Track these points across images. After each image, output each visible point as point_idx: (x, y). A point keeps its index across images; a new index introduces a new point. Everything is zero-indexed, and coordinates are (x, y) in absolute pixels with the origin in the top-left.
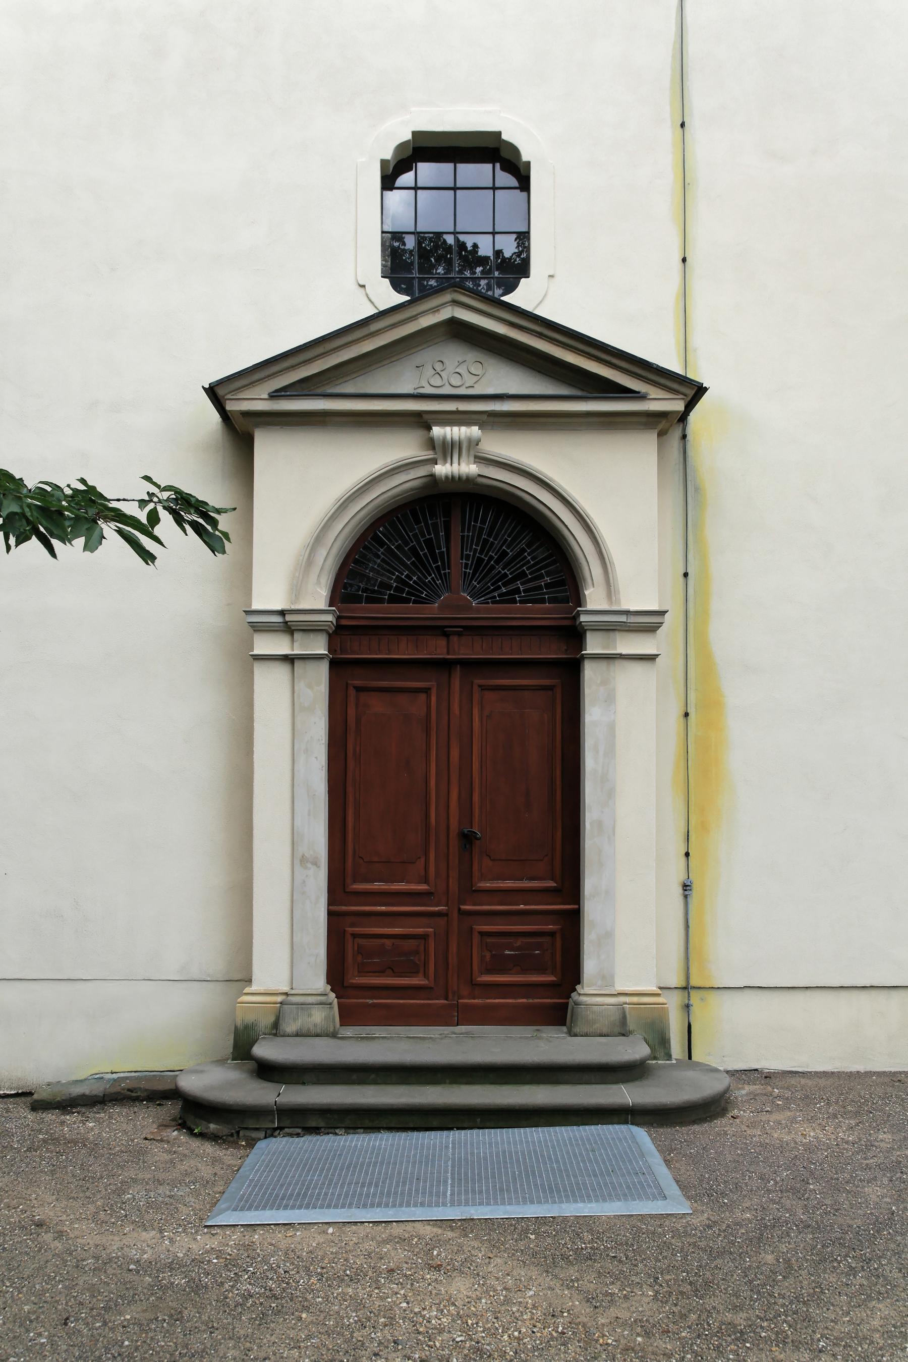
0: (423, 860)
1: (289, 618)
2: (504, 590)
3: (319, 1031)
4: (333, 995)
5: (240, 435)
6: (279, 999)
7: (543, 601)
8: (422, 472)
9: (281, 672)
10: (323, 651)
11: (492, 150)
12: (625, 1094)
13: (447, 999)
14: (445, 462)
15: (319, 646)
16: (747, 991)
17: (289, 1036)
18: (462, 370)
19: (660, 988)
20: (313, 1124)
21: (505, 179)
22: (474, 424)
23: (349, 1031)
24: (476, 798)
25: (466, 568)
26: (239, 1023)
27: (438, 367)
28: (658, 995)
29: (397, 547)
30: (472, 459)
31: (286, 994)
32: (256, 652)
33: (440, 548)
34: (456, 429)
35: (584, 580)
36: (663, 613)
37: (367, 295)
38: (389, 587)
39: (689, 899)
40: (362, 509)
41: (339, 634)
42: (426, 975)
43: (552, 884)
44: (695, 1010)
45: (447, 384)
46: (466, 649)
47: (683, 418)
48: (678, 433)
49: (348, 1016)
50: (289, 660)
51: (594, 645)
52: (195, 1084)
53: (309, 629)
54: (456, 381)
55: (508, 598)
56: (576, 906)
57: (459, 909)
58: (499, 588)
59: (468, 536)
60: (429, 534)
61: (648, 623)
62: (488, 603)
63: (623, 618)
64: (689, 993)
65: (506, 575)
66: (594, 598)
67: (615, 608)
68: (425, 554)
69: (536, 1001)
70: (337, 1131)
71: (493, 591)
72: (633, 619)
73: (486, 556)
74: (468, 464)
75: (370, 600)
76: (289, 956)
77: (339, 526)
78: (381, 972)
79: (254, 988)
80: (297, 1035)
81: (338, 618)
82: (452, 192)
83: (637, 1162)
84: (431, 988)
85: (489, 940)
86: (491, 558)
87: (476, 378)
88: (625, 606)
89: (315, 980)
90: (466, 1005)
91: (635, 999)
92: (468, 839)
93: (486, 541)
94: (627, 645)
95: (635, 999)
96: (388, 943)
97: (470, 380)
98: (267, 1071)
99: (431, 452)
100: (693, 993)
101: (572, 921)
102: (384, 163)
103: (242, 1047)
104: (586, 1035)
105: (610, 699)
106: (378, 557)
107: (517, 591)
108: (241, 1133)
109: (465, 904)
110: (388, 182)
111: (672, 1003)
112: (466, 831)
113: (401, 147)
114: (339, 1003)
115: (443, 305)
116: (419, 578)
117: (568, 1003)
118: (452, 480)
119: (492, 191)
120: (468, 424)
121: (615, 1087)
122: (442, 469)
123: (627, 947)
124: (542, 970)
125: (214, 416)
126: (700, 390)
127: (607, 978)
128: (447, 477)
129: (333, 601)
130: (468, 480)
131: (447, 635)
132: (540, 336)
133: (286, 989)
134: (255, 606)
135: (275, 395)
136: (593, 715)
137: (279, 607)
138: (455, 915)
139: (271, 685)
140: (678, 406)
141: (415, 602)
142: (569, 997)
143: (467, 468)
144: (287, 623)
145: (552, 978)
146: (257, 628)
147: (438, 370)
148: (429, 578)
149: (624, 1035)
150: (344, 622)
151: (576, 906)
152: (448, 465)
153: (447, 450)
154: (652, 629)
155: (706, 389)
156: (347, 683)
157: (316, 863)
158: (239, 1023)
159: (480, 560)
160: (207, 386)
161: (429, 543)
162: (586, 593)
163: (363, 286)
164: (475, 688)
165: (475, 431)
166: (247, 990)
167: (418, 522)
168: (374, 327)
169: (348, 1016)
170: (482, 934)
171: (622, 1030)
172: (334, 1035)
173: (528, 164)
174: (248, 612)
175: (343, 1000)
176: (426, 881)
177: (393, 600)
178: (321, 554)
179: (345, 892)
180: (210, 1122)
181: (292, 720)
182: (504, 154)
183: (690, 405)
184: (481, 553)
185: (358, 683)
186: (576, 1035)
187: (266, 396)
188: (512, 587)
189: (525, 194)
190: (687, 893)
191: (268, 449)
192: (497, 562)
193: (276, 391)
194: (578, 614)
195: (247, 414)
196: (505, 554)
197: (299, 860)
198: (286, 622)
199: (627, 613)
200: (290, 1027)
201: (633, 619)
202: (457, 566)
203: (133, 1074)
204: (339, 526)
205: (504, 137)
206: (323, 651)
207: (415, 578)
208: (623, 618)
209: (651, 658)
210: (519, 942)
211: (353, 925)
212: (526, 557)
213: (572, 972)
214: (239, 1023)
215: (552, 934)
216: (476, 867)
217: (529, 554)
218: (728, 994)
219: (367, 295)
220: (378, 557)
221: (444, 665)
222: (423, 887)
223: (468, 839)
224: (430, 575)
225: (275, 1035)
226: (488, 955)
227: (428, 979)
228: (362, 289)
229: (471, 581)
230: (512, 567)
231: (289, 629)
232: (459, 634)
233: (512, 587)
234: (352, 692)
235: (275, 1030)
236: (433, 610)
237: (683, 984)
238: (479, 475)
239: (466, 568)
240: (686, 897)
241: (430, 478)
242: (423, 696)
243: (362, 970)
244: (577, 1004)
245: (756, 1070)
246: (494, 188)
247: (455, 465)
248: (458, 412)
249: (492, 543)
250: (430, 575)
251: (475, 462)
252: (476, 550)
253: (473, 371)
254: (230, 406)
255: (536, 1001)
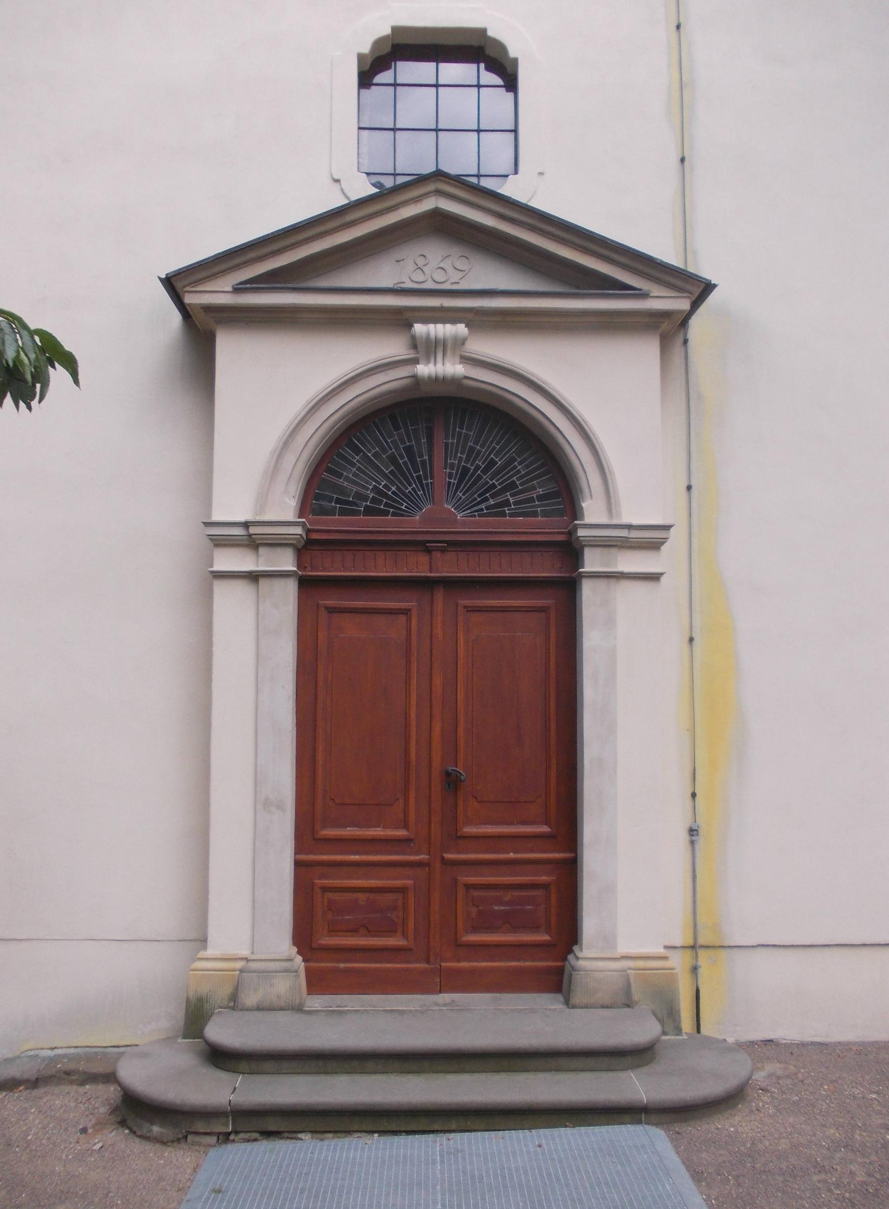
0: (401, 801)
1: (253, 530)
2: (492, 502)
3: (283, 1004)
4: (299, 959)
5: (200, 334)
6: (239, 965)
7: (535, 514)
8: (403, 372)
9: (241, 591)
10: (291, 567)
11: (475, 49)
12: (635, 1086)
13: (428, 962)
14: (428, 362)
15: (286, 561)
16: (759, 950)
17: (248, 1010)
18: (446, 264)
19: (666, 947)
20: (272, 1128)
21: (489, 78)
22: (460, 322)
23: (316, 1002)
24: (461, 731)
25: (450, 478)
26: (191, 994)
27: (421, 262)
28: (665, 958)
29: (376, 455)
30: (457, 359)
31: (247, 959)
32: (216, 568)
33: (421, 456)
34: (440, 326)
35: (581, 492)
36: (667, 528)
37: (342, 190)
38: (365, 498)
39: (697, 847)
40: (336, 411)
41: (306, 549)
42: (404, 935)
43: (545, 829)
44: (703, 972)
45: (430, 279)
46: (450, 567)
47: (684, 321)
48: (681, 339)
49: (317, 982)
50: (254, 577)
51: (592, 561)
52: (136, 1075)
53: (275, 543)
54: (439, 276)
55: (498, 510)
56: (572, 855)
57: (443, 858)
58: (487, 499)
59: (452, 443)
60: (410, 441)
61: (651, 539)
62: (475, 516)
63: (624, 533)
64: (697, 954)
65: (494, 486)
66: (593, 511)
67: (615, 522)
68: (405, 463)
69: (528, 964)
70: (299, 1135)
71: (479, 503)
72: (634, 534)
73: (472, 465)
74: (454, 364)
75: (343, 512)
76: (250, 914)
77: (309, 430)
78: (354, 931)
79: (210, 952)
80: (259, 1008)
81: (308, 531)
82: (434, 89)
83: (663, 1185)
84: (411, 950)
85: (476, 893)
86: (478, 468)
87: (461, 274)
88: (626, 520)
89: (280, 943)
90: (451, 970)
91: (641, 964)
92: (452, 782)
93: (472, 449)
94: (629, 562)
95: (641, 964)
96: (362, 897)
97: (455, 276)
98: (221, 1057)
99: (412, 351)
100: (702, 953)
101: (569, 872)
102: (361, 58)
103: (195, 1016)
104: (586, 1007)
105: (610, 622)
106: (353, 465)
107: (507, 503)
108: (189, 1137)
109: (448, 852)
110: (366, 79)
111: (678, 963)
112: (450, 769)
113: (378, 43)
114: (308, 970)
115: (426, 195)
116: (398, 488)
117: (564, 966)
118: (436, 380)
119: (476, 89)
120: (454, 322)
121: (622, 1075)
122: (424, 370)
123: (631, 900)
124: (535, 928)
125: (176, 317)
126: (708, 288)
127: (610, 940)
128: (430, 377)
129: (303, 511)
130: (455, 382)
131: (429, 551)
132: (532, 229)
133: (245, 952)
134: (216, 517)
135: (238, 290)
136: (592, 640)
137: (242, 518)
138: (438, 865)
139: (233, 606)
140: (683, 305)
141: (394, 514)
142: (565, 959)
143: (450, 368)
144: (251, 538)
145: (546, 938)
146: (220, 542)
147: (420, 265)
148: (410, 489)
149: (629, 1006)
150: (315, 536)
151: (572, 855)
152: (431, 366)
153: (431, 348)
154: (655, 546)
155: (715, 286)
156: (318, 605)
157: (281, 807)
158: (191, 994)
159: (465, 470)
160: (164, 276)
161: (409, 450)
162: (584, 505)
163: (337, 181)
164: (461, 610)
165: (461, 329)
166: (202, 954)
167: (397, 428)
168: (349, 217)
169: (317, 982)
170: (468, 887)
171: (625, 1000)
172: (299, 1009)
173: (515, 62)
174: (208, 524)
175: (311, 964)
176: (406, 826)
177: (369, 511)
178: (290, 459)
179: (314, 839)
180: (152, 1123)
181: (256, 644)
182: (490, 52)
183: (696, 304)
184: (467, 461)
185: (330, 603)
186: (574, 1007)
187: (230, 289)
188: (500, 499)
189: (511, 95)
190: (694, 838)
191: (233, 351)
192: (485, 471)
193: (240, 283)
194: (576, 528)
195: (209, 309)
196: (492, 463)
197: (263, 805)
198: (250, 535)
199: (629, 527)
200: (250, 998)
201: (634, 534)
202: (442, 475)
203: (72, 1051)
204: (309, 430)
205: (490, 33)
206: (291, 567)
207: (394, 489)
208: (624, 533)
209: (654, 577)
210: (509, 896)
211: (322, 877)
212: (515, 467)
213: (568, 932)
214: (191, 994)
215: (545, 886)
216: (460, 808)
217: (520, 464)
218: (735, 950)
219: (342, 190)
220: (353, 465)
221: (426, 585)
222: (401, 833)
223: (452, 782)
224: (410, 485)
225: (233, 1008)
226: (474, 910)
227: (407, 939)
228: (337, 185)
229: (455, 493)
230: (501, 478)
231: (253, 543)
232: (443, 551)
233: (500, 499)
234: (323, 614)
235: (234, 1002)
236: (415, 522)
237: (691, 942)
238: (466, 378)
239: (450, 478)
240: (692, 843)
241: (412, 379)
242: (402, 618)
243: (334, 929)
244: (573, 968)
245: (771, 1041)
246: (479, 86)
247: (439, 365)
248: (442, 309)
249: (479, 452)
250: (410, 485)
251: (461, 363)
252: (461, 458)
253: (458, 266)
254: (189, 299)
255: (528, 964)
